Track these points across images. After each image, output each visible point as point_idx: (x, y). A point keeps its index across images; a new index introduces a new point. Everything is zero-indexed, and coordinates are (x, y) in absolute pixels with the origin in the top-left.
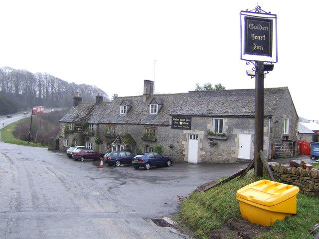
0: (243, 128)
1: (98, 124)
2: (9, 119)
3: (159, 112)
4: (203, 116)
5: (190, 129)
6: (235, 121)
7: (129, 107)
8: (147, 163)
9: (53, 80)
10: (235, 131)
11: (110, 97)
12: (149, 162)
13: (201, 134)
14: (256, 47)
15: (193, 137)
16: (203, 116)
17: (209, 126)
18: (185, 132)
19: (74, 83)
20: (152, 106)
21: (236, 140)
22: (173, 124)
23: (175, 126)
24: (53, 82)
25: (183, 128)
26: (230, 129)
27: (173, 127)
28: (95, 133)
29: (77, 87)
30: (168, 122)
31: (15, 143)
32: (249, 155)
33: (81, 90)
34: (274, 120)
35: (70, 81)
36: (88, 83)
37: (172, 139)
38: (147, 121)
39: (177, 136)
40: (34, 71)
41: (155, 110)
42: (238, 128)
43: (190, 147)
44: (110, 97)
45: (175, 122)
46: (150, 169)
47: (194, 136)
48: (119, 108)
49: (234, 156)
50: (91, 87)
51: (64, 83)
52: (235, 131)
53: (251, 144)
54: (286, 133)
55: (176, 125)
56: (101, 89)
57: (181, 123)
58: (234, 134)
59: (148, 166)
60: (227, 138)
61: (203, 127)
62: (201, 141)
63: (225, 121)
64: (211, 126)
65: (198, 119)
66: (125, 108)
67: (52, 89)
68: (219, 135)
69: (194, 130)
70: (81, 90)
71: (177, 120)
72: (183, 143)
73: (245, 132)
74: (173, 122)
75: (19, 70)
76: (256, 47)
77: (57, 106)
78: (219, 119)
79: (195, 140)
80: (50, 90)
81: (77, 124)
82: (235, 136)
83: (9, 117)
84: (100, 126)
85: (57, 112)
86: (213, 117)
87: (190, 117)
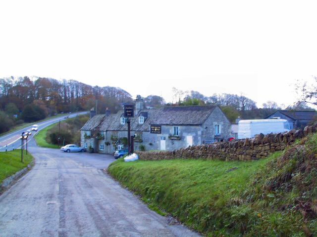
0: (189, 132)
3: (144, 122)
4: (167, 125)
5: (160, 133)
6: (184, 127)
9: (79, 85)
10: (184, 134)
14: (128, 114)
16: (167, 125)
17: (171, 131)
18: (158, 135)
19: (97, 87)
21: (185, 140)
22: (151, 130)
23: (152, 131)
24: (77, 86)
25: (157, 132)
26: (181, 133)
27: (151, 132)
28: (105, 137)
29: (101, 90)
31: (49, 147)
33: (105, 92)
34: (205, 127)
35: (93, 85)
36: (111, 86)
38: (136, 128)
39: (154, 138)
42: (186, 132)
43: (161, 144)
48: (120, 119)
50: (115, 88)
51: (85, 88)
57: (156, 130)
60: (180, 138)
61: (168, 131)
64: (172, 131)
65: (165, 126)
67: (77, 94)
68: (175, 137)
70: (105, 92)
71: (153, 127)
72: (158, 142)
74: (151, 129)
75: (44, 78)
76: (128, 114)
77: (81, 109)
78: (176, 126)
80: (75, 95)
81: (92, 132)
82: (184, 137)
85: (81, 117)
87: (160, 126)
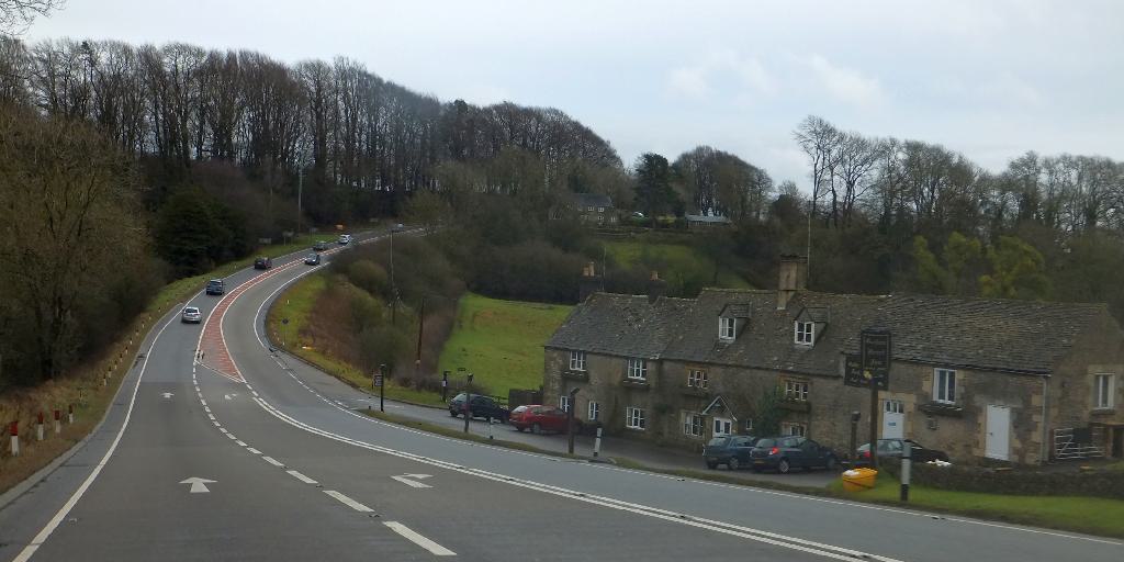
0: (998, 395)
1: (660, 362)
2: (264, 276)
7: (743, 322)
8: (783, 458)
10: (978, 400)
11: (630, 160)
12: (787, 457)
13: (910, 401)
15: (892, 408)
17: (926, 386)
20: (801, 327)
26: (967, 397)
27: (847, 382)
30: (836, 366)
32: (1007, 452)
37: (847, 409)
40: (288, 52)
41: (809, 337)
44: (630, 160)
45: (853, 371)
46: (788, 473)
47: (895, 404)
49: (977, 452)
52: (978, 400)
53: (1010, 433)
54: (1105, 401)
55: (855, 377)
56: (585, 123)
58: (978, 404)
59: (785, 466)
61: (914, 386)
62: (909, 417)
63: (959, 375)
66: (731, 324)
69: (893, 392)
73: (997, 402)
74: (848, 369)
79: (902, 415)
83: (261, 267)
84: (667, 366)
86: (937, 365)
